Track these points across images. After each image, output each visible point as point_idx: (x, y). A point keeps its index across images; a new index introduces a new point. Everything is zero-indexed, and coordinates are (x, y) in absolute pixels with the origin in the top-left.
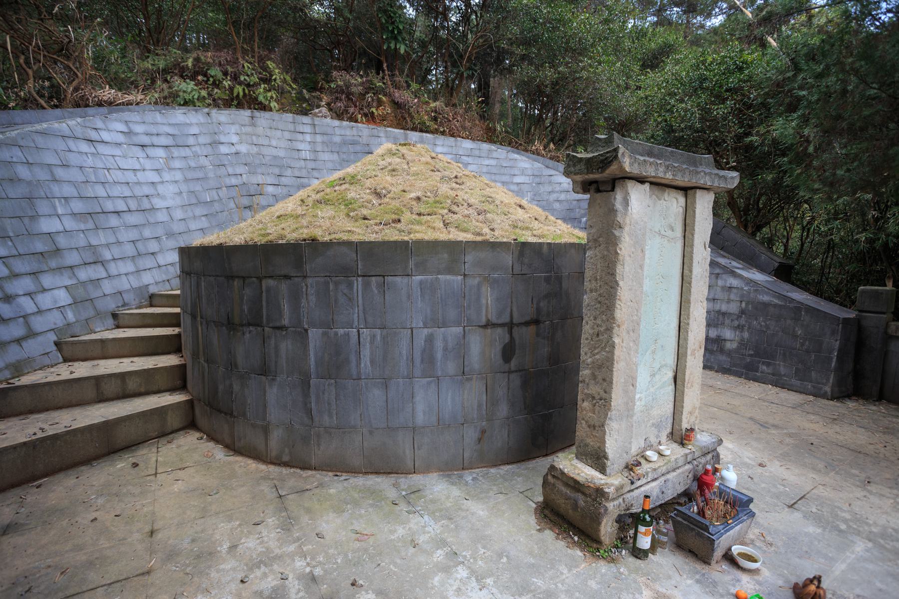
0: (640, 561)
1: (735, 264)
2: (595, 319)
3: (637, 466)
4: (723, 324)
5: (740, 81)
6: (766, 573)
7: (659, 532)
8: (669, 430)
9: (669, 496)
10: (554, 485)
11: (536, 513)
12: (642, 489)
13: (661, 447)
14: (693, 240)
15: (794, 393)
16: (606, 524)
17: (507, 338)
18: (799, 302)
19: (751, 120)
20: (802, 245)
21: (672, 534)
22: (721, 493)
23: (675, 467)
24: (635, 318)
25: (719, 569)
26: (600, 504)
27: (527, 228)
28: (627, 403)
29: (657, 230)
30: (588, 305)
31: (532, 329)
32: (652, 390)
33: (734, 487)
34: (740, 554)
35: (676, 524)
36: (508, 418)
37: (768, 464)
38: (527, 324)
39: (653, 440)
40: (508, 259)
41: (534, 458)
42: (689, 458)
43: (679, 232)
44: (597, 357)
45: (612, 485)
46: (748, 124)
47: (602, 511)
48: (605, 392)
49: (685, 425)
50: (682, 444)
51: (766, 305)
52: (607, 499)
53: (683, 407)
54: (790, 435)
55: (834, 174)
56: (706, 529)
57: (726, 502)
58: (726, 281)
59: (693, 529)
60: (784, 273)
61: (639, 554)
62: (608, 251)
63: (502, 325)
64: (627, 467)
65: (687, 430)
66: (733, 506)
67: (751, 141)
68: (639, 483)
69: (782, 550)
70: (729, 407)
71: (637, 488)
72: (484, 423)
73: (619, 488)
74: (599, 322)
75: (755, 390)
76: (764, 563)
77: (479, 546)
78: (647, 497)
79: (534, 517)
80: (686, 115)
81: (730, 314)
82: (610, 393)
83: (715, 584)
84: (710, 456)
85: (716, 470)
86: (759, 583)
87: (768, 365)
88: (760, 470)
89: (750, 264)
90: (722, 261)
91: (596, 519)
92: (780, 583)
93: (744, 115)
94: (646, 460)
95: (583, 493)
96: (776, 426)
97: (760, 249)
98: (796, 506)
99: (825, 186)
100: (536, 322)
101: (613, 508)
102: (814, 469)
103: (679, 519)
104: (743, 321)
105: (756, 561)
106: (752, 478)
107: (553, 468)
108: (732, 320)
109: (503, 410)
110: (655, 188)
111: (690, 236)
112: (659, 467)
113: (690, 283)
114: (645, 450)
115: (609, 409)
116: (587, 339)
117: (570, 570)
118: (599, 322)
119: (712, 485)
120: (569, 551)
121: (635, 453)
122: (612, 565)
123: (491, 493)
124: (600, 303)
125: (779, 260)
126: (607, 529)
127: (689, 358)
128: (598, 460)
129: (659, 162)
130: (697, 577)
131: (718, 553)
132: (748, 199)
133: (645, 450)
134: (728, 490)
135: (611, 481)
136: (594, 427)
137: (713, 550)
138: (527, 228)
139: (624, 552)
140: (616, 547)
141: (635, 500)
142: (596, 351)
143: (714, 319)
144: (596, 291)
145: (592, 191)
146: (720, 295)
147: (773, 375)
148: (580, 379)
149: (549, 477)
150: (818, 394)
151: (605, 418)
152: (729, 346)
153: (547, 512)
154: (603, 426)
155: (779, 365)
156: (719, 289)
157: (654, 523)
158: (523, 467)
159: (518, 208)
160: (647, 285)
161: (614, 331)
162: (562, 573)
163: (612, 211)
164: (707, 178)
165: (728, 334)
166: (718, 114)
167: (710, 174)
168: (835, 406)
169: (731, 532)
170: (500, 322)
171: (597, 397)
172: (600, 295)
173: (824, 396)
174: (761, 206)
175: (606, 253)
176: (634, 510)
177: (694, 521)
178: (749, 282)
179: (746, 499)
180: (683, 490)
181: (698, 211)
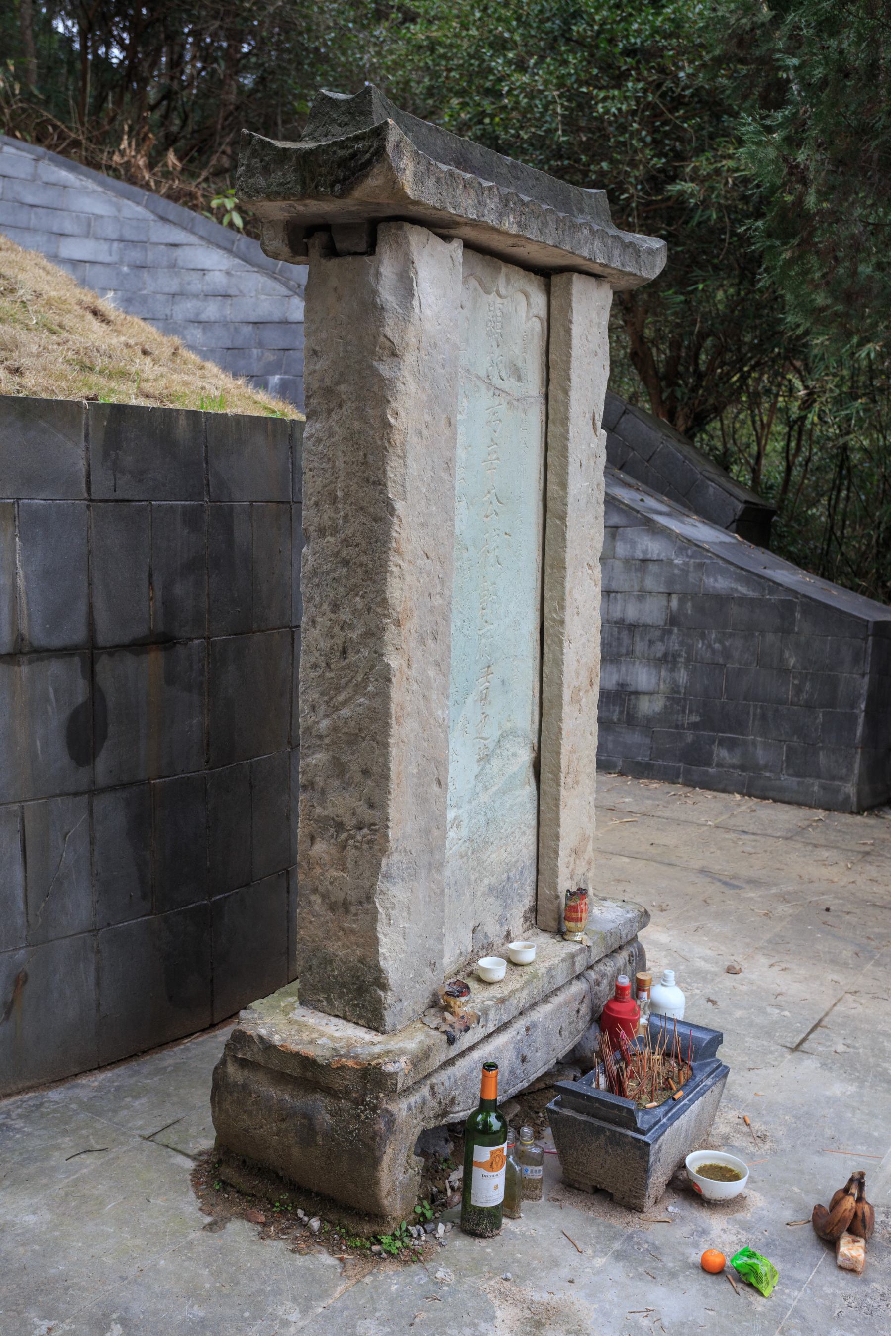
0: (483, 1242)
1: (651, 502)
2: (335, 608)
3: (461, 994)
4: (630, 653)
5: (656, 31)
6: (758, 1201)
7: (522, 1157)
8: (528, 901)
9: (540, 1064)
10: (245, 1087)
11: (196, 1184)
12: (476, 1055)
13: (512, 946)
14: (566, 405)
15: (786, 807)
16: (393, 1160)
17: (81, 693)
18: (788, 590)
19: (679, 139)
20: (789, 469)
21: (553, 1162)
22: (654, 1035)
23: (548, 989)
24: (438, 601)
25: (663, 1216)
26: (374, 1109)
27: (123, 375)
28: (427, 832)
29: (482, 373)
30: (315, 572)
31: (153, 661)
32: (484, 797)
33: (679, 1016)
34: (703, 1170)
35: (558, 1124)
36: (94, 931)
37: (745, 965)
38: (138, 646)
39: (493, 930)
40: (74, 454)
41: (177, 1040)
42: (580, 963)
43: (533, 385)
44: (345, 712)
45: (402, 1052)
46: (673, 149)
47: (381, 1125)
48: (371, 806)
49: (565, 884)
50: (561, 933)
51: (722, 600)
52: (393, 1093)
53: (557, 837)
54: (784, 898)
55: (854, 273)
56: (628, 1119)
57: (667, 1055)
58: (633, 544)
59: (601, 1130)
60: (756, 525)
61: (478, 1223)
62: (363, 419)
63: (64, 652)
64: (434, 1004)
65: (571, 895)
66: (682, 1061)
67: (682, 193)
68: (467, 1040)
69: (786, 1145)
70: (653, 850)
71: (462, 1055)
72: (21, 955)
73: (420, 1059)
74: (345, 615)
75: (706, 807)
76: (752, 1180)
77: (33, 1315)
78: (489, 1067)
79: (191, 1195)
80: (530, 108)
81: (645, 626)
82: (384, 806)
83: (655, 1252)
84: (625, 954)
85: (640, 986)
86: (746, 1227)
87: (731, 745)
88: (729, 981)
89: (684, 505)
90: (625, 495)
91: (367, 1154)
92: (788, 1215)
93: (664, 124)
94: (480, 980)
95: (329, 1091)
96: (754, 882)
97: (705, 469)
98: (806, 1045)
99: (836, 299)
100: (165, 641)
101: (408, 1113)
102: (834, 961)
103: (567, 1112)
104: (674, 643)
105: (736, 1177)
106: (714, 1003)
107: (240, 1039)
108: (651, 643)
109: (79, 907)
110: (475, 257)
111: (561, 396)
112: (513, 992)
113: (563, 518)
114: (475, 956)
115: (383, 851)
116: (315, 666)
117: (305, 1311)
118: (345, 615)
119: (635, 1022)
120: (300, 1261)
121: (453, 969)
122: (414, 1267)
123: (57, 1158)
124: (346, 562)
125: (744, 496)
126: (396, 1175)
127: (568, 710)
128: (360, 994)
129: (486, 184)
130: (617, 1246)
131: (659, 1177)
132: (675, 345)
133: (475, 956)
134: (670, 1026)
135: (399, 1045)
136: (346, 905)
137: (647, 1171)
138: (123, 375)
139: (441, 1228)
140: (421, 1220)
141: (461, 1086)
142: (341, 698)
143: (618, 641)
144: (335, 531)
145: (315, 253)
146: (622, 581)
147: (743, 768)
148: (302, 779)
149: (231, 1069)
150: (832, 805)
151: (375, 875)
152: (648, 707)
153: (227, 1172)
154: (369, 898)
155: (754, 743)
156: (618, 565)
157: (511, 1135)
158: (145, 1070)
159: (89, 316)
160: (464, 517)
161: (387, 637)
162: (285, 1323)
163: (371, 309)
164: (597, 243)
165: (643, 677)
166: (607, 112)
167: (603, 234)
168: (866, 826)
169: (683, 1119)
170: (56, 642)
171: (350, 822)
172: (346, 542)
173: (843, 807)
174: (703, 368)
175: (357, 425)
176: (460, 1114)
177: (597, 1120)
178: (686, 544)
179: (707, 1037)
180: (568, 1048)
181: (576, 330)
